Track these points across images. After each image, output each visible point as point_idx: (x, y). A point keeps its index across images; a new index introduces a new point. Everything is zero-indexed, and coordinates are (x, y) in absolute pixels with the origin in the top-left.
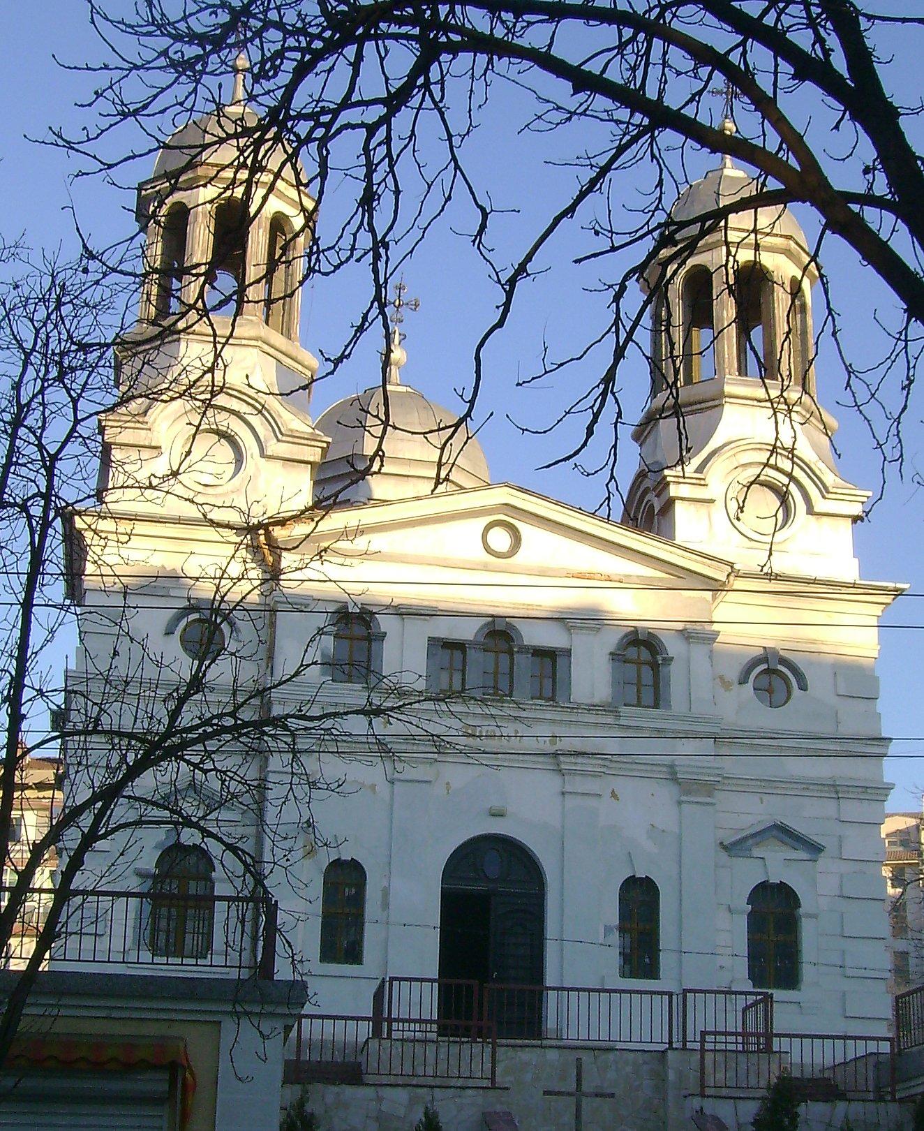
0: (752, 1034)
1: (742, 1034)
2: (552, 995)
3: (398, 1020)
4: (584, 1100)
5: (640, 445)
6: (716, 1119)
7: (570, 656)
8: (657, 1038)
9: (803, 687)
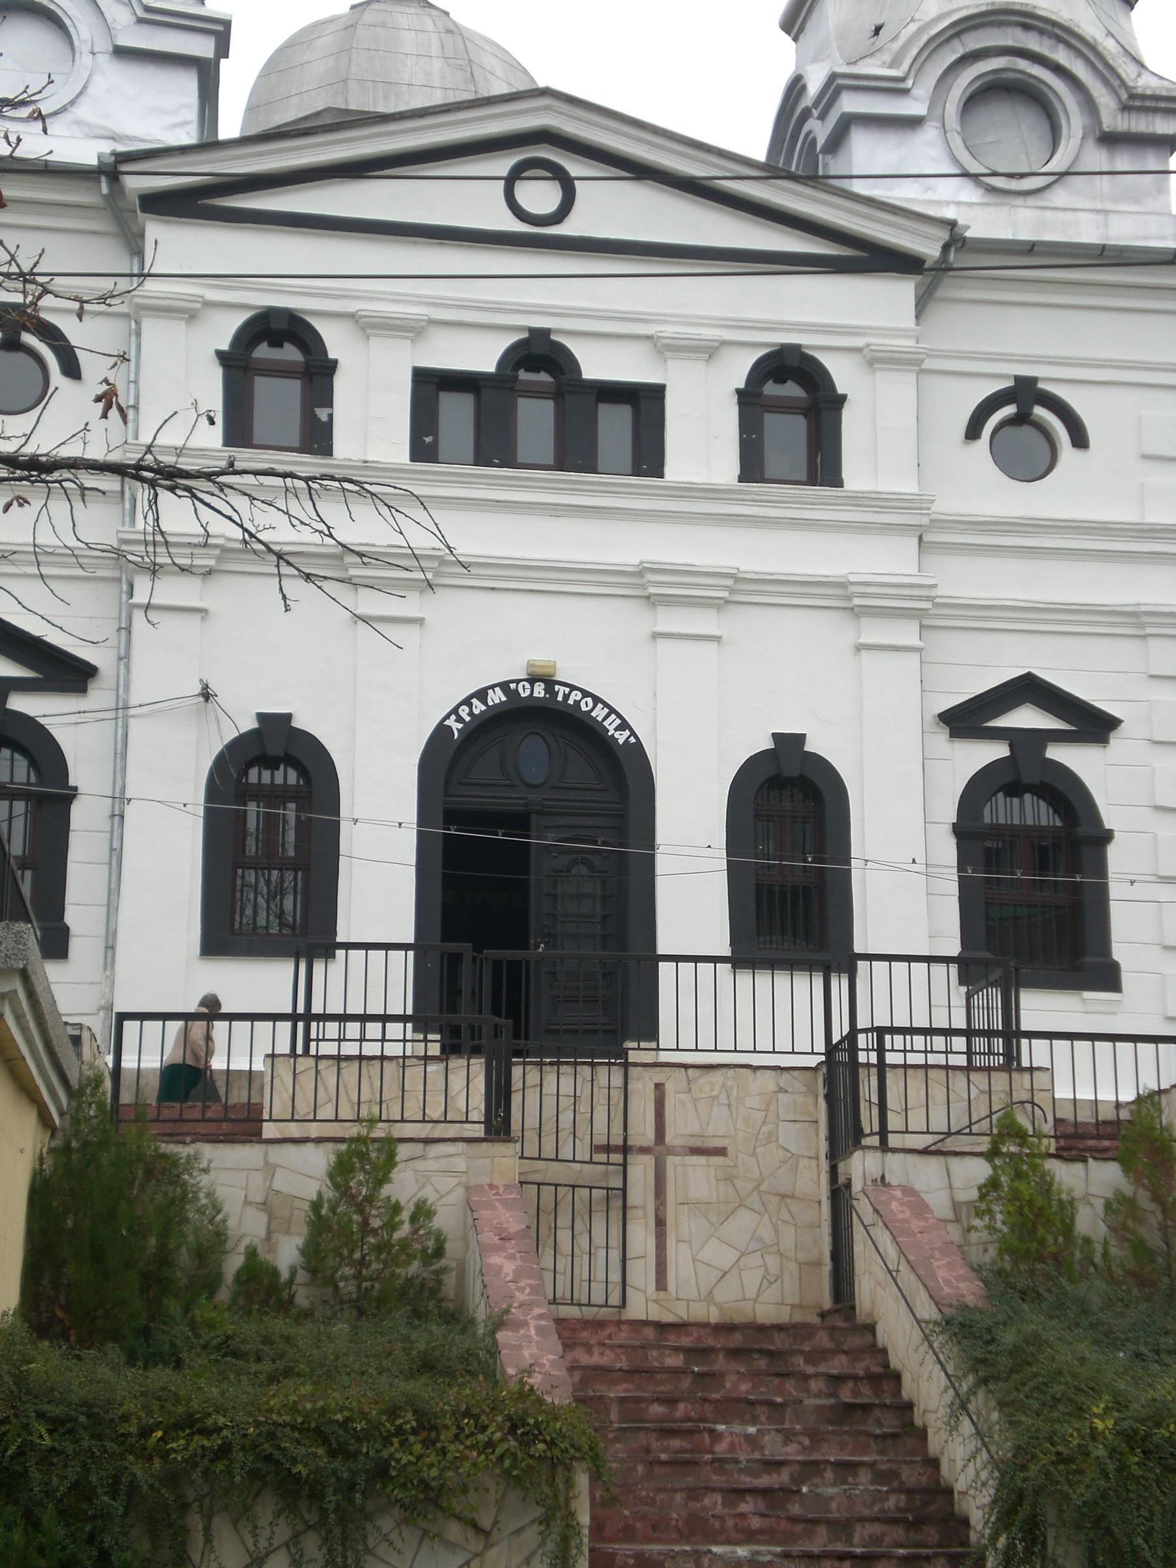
0: (981, 1033)
1: (969, 1033)
2: (665, 969)
3: (325, 1017)
4: (671, 1162)
5: (795, 39)
6: (908, 1191)
7: (812, 481)
8: (803, 1045)
9: (1080, 439)
